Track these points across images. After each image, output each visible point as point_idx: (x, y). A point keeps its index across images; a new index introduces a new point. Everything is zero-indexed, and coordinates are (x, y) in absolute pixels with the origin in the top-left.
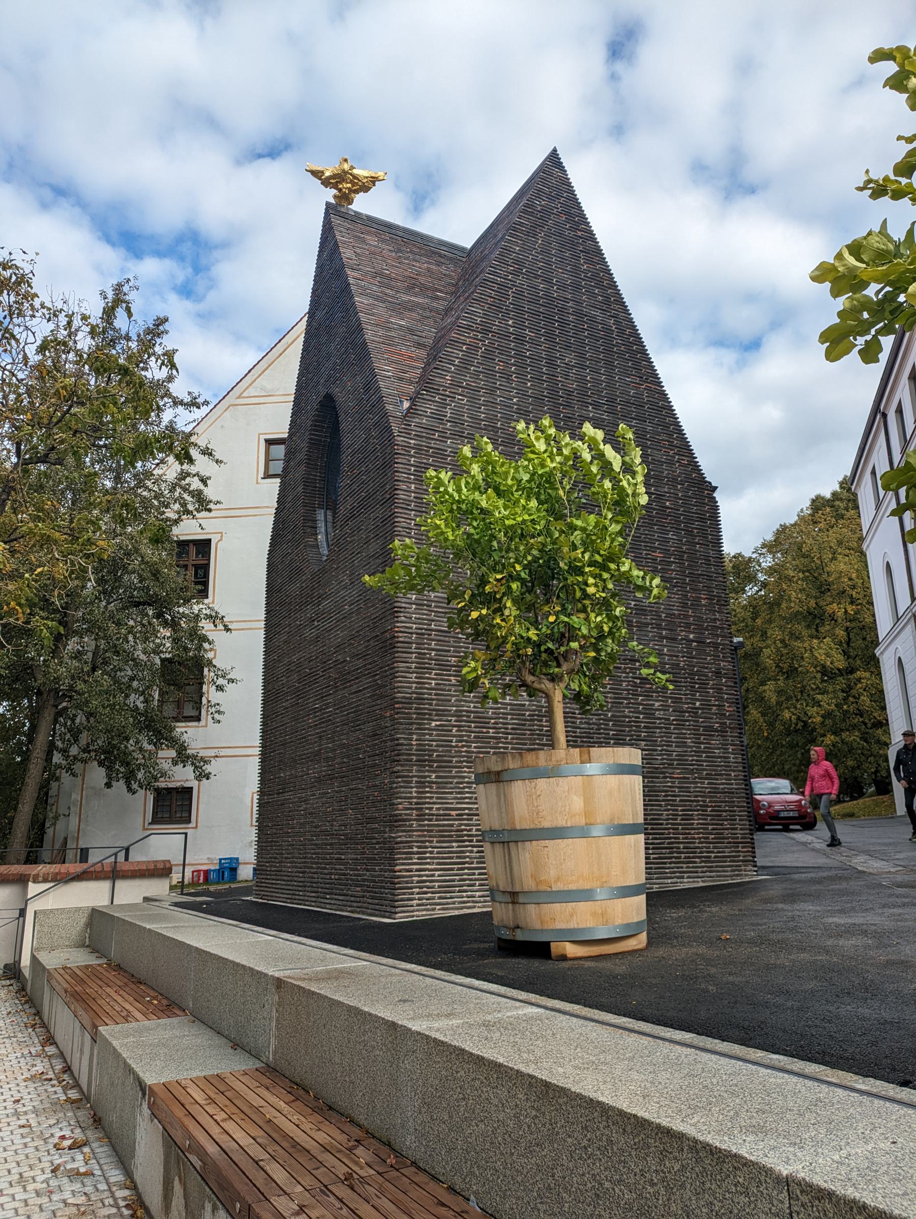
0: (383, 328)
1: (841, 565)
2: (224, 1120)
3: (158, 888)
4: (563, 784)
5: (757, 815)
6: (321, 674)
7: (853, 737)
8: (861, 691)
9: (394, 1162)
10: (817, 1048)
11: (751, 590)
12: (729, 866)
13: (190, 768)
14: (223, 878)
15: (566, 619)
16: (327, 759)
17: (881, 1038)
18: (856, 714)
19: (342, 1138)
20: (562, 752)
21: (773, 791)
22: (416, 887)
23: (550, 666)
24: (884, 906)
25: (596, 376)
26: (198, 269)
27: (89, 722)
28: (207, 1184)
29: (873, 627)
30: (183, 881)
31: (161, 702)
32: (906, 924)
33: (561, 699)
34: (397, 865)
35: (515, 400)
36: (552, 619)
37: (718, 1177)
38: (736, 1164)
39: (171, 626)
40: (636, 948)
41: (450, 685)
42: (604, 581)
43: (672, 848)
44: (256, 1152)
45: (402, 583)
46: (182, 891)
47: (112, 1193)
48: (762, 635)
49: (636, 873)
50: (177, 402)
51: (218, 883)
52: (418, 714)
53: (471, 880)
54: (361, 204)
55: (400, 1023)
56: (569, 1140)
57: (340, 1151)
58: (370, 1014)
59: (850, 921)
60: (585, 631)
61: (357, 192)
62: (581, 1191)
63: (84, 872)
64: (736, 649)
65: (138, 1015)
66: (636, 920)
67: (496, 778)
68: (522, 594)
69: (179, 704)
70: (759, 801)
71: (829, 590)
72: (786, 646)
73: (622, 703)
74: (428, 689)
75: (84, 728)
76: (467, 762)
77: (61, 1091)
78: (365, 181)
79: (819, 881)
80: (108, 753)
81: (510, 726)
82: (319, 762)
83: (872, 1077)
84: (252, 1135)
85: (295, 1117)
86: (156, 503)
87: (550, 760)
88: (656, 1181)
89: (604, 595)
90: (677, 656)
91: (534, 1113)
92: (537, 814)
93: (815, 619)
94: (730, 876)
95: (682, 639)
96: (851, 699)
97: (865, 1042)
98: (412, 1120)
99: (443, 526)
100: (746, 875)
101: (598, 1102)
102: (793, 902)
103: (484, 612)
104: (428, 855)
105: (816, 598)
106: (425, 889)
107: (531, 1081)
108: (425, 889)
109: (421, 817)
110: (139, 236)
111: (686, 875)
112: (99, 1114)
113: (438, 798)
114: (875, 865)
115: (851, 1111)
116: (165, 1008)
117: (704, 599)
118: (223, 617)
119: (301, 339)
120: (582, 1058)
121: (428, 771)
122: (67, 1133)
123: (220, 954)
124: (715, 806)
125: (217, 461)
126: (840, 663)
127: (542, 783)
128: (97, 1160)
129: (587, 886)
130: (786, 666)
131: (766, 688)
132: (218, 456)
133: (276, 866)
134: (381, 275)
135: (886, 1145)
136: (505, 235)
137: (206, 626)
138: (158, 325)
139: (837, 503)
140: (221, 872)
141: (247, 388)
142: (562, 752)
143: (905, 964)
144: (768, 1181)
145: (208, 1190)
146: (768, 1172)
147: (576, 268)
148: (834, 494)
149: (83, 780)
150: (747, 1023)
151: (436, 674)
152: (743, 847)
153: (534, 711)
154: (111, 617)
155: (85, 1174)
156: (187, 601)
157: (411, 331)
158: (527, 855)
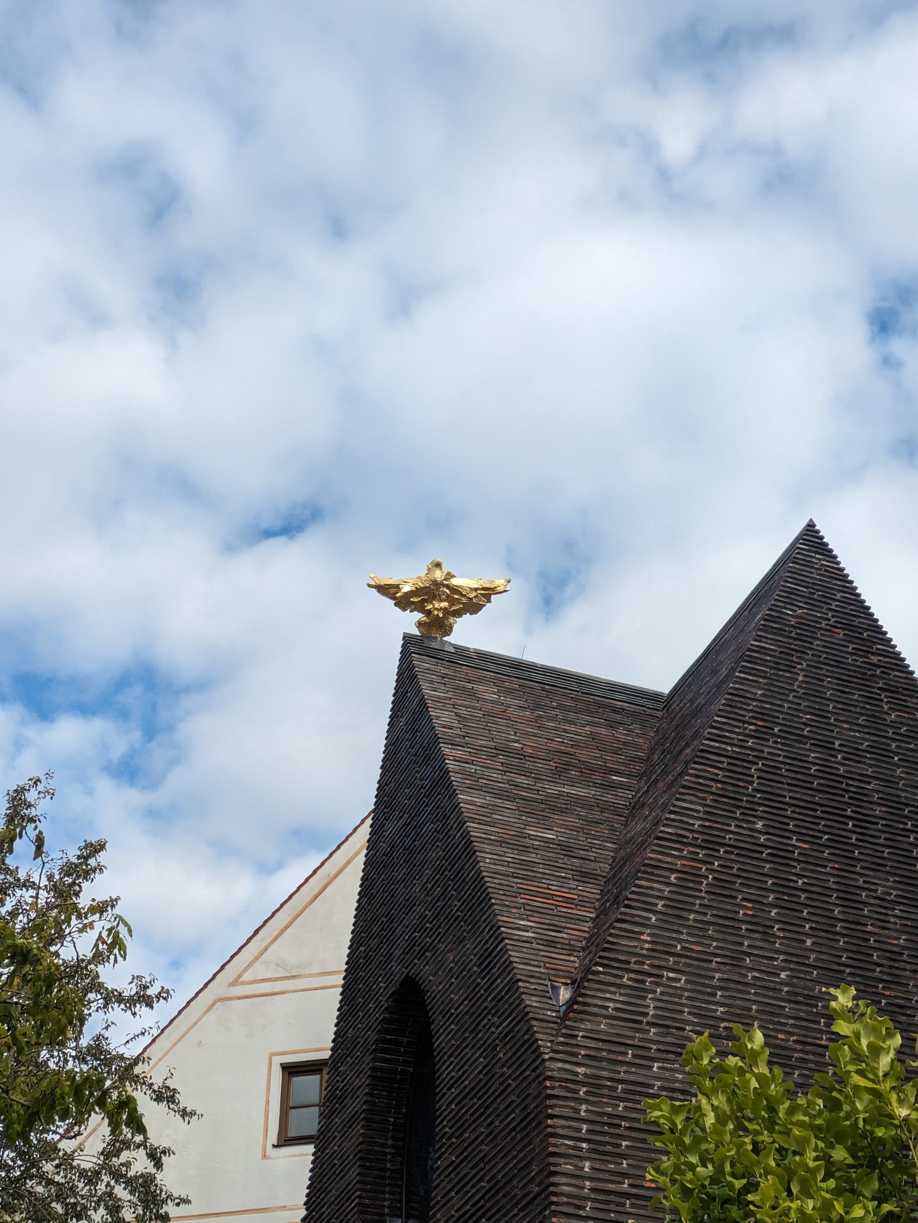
0: (513, 846)
26: (151, 731)
50: (111, 998)
54: (466, 633)
61: (458, 614)
78: (472, 595)
86: (59, 1208)
110: (51, 680)
125: (184, 1113)
136: (733, 670)
138: (86, 858)
141: (250, 965)
147: (876, 719)
157: (567, 850)
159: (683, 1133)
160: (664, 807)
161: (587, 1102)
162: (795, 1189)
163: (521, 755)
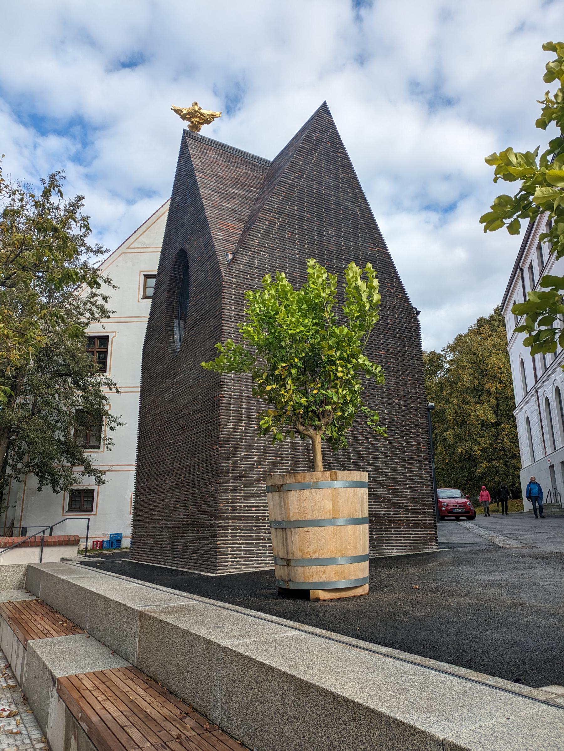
0: (217, 208)
1: (494, 360)
2: (104, 700)
3: (71, 552)
4: (319, 493)
5: (440, 510)
6: (175, 422)
7: (499, 464)
8: (505, 436)
9: (208, 727)
10: (467, 658)
11: (440, 374)
12: (421, 543)
13: (93, 478)
14: (112, 547)
15: (324, 392)
16: (177, 475)
17: (505, 652)
18: (501, 450)
19: (177, 712)
20: (320, 474)
21: (451, 496)
22: (230, 554)
23: (314, 421)
24: (513, 569)
25: (347, 242)
26: (85, 144)
27: (29, 448)
28: (91, 741)
29: (512, 398)
30: (86, 548)
31: (76, 436)
32: (525, 580)
33: (320, 441)
34: (218, 540)
35: (297, 256)
36: (315, 392)
37: (402, 740)
38: (412, 732)
39: (83, 389)
40: (362, 594)
41: (253, 430)
42: (349, 369)
43: (387, 531)
44: (123, 721)
45: (226, 366)
46: (86, 554)
47: (33, 745)
48: (446, 401)
49: (363, 548)
50: (89, 250)
51: (109, 549)
52: (233, 447)
53: (264, 550)
54: (205, 131)
55: (214, 641)
56: (314, 715)
57: (175, 720)
58: (196, 635)
59: (492, 578)
60: (335, 399)
61: (203, 124)
62: (320, 747)
63: (24, 542)
64: (429, 409)
65: (54, 633)
66: (362, 577)
67: (279, 489)
68: (298, 376)
69: (87, 438)
70: (441, 502)
71: (487, 375)
72: (460, 408)
73: (359, 443)
74: (240, 432)
75: (26, 452)
76: (263, 478)
77: (4, 680)
78: (208, 117)
79: (475, 552)
80: (41, 467)
81: (290, 456)
82: (172, 476)
83: (498, 676)
84: (121, 710)
85: (149, 699)
86: (74, 312)
87: (312, 478)
88: (365, 741)
89: (347, 378)
90: (393, 415)
91: (293, 698)
92: (304, 511)
93: (478, 392)
94: (422, 549)
95: (396, 404)
96: (498, 441)
97: (496, 654)
98: (220, 701)
99: (252, 332)
100: (431, 548)
101: (332, 692)
102: (459, 565)
103: (274, 386)
104: (238, 534)
105: (479, 379)
106: (235, 556)
107: (292, 679)
108: (235, 556)
109: (234, 511)
111: (395, 548)
112: (27, 696)
113: (244, 500)
114: (509, 543)
115: (484, 698)
116: (71, 628)
117: (410, 380)
118: (115, 384)
119: (167, 214)
120: (324, 664)
121: (239, 483)
122: (6, 707)
123: (106, 596)
124: (414, 506)
125: (114, 287)
126: (492, 418)
127: (307, 492)
128: (25, 724)
129: (333, 556)
130: (460, 420)
131: (448, 433)
132: (114, 283)
133: (144, 540)
134: (217, 175)
135: (503, 720)
136: (293, 154)
137: (105, 390)
138: (78, 201)
139: (493, 322)
140: (111, 542)
142: (320, 474)
143: (522, 606)
144: (431, 742)
145: (92, 745)
146: (431, 737)
148: (491, 317)
149: (25, 484)
150: (425, 642)
151: (245, 423)
152: (430, 531)
153: (305, 446)
154: (44, 383)
155: (17, 733)
156: (93, 374)
157: (234, 211)
158: (297, 536)
159: (259, 299)
160: (267, 199)
161: (235, 289)
162: (289, 316)
163: (221, 177)
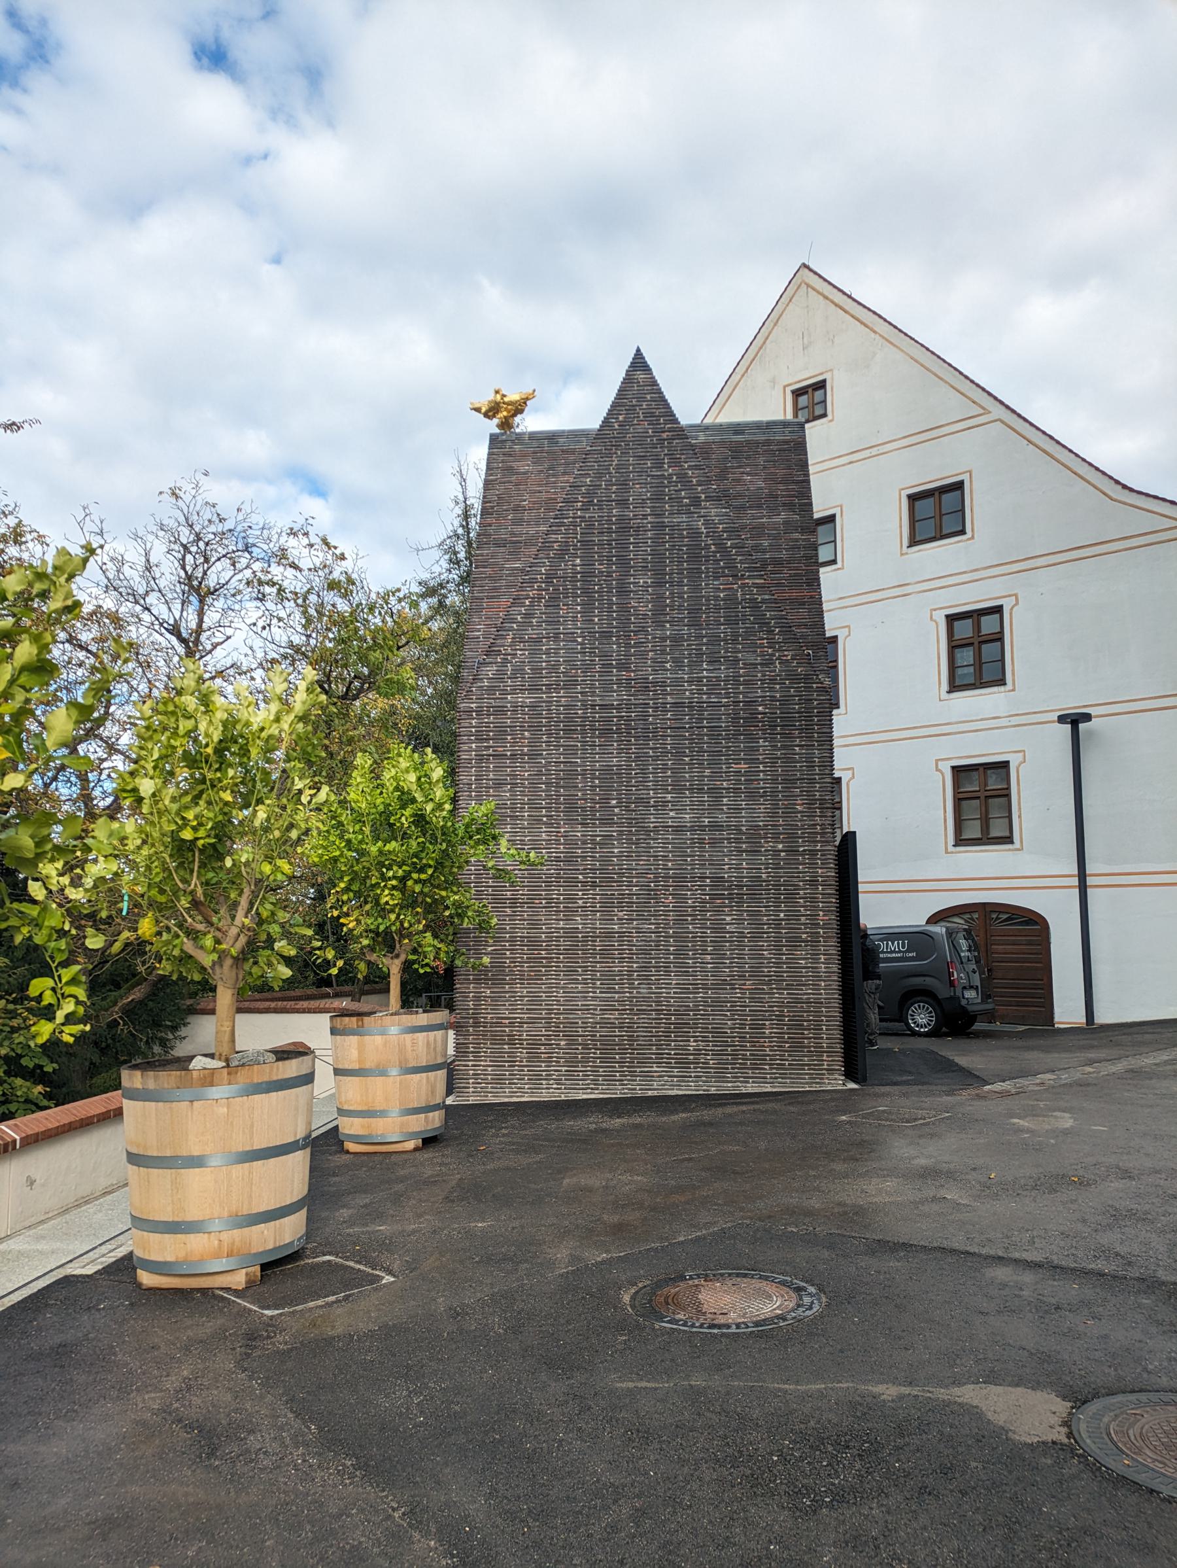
54: (528, 423)
61: (514, 415)
